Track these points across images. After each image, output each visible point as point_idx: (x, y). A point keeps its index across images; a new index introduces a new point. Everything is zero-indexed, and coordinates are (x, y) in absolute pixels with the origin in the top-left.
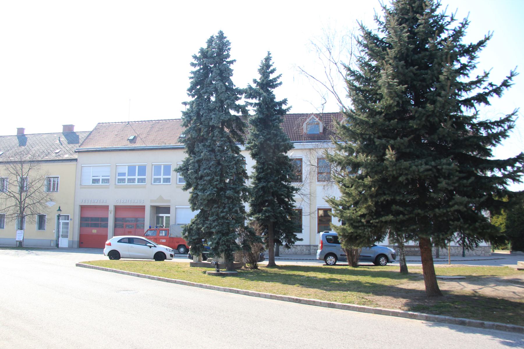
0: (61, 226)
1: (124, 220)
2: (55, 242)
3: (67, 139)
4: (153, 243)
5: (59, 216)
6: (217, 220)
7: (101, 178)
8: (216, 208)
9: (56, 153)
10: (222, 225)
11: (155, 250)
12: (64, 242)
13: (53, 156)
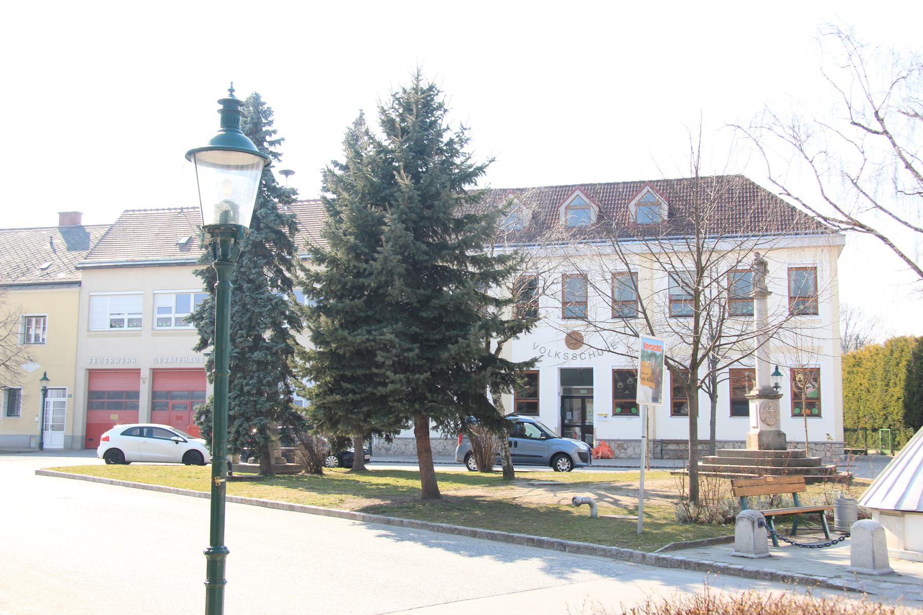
0: (51, 409)
1: (169, 395)
2: (38, 439)
3: (67, 241)
4: (182, 436)
5: (45, 391)
6: (238, 396)
7: (126, 318)
8: (240, 378)
9: (43, 269)
10: (246, 404)
11: (184, 448)
12: (54, 439)
13: (35, 276)
